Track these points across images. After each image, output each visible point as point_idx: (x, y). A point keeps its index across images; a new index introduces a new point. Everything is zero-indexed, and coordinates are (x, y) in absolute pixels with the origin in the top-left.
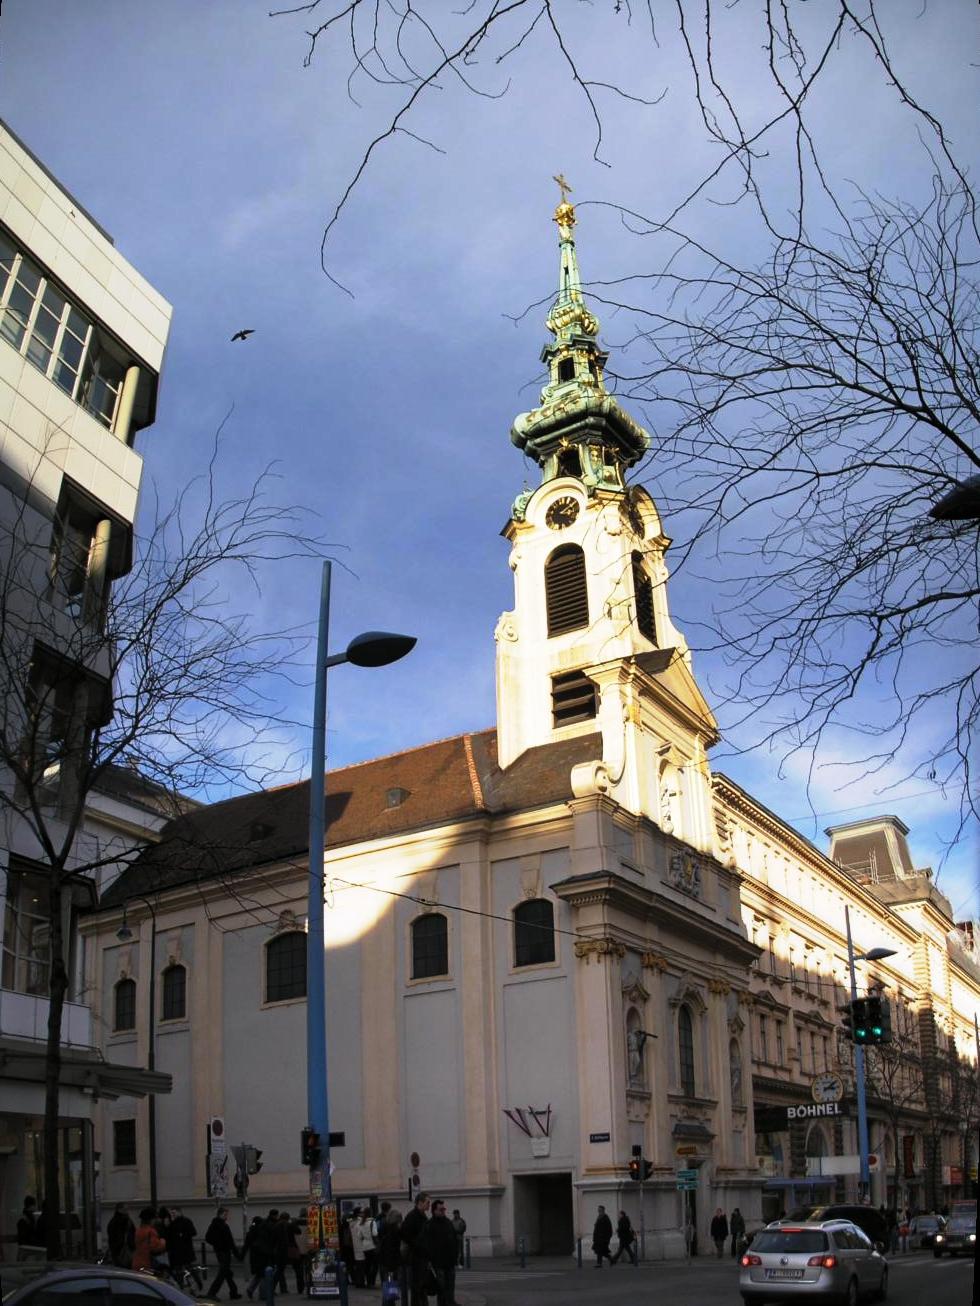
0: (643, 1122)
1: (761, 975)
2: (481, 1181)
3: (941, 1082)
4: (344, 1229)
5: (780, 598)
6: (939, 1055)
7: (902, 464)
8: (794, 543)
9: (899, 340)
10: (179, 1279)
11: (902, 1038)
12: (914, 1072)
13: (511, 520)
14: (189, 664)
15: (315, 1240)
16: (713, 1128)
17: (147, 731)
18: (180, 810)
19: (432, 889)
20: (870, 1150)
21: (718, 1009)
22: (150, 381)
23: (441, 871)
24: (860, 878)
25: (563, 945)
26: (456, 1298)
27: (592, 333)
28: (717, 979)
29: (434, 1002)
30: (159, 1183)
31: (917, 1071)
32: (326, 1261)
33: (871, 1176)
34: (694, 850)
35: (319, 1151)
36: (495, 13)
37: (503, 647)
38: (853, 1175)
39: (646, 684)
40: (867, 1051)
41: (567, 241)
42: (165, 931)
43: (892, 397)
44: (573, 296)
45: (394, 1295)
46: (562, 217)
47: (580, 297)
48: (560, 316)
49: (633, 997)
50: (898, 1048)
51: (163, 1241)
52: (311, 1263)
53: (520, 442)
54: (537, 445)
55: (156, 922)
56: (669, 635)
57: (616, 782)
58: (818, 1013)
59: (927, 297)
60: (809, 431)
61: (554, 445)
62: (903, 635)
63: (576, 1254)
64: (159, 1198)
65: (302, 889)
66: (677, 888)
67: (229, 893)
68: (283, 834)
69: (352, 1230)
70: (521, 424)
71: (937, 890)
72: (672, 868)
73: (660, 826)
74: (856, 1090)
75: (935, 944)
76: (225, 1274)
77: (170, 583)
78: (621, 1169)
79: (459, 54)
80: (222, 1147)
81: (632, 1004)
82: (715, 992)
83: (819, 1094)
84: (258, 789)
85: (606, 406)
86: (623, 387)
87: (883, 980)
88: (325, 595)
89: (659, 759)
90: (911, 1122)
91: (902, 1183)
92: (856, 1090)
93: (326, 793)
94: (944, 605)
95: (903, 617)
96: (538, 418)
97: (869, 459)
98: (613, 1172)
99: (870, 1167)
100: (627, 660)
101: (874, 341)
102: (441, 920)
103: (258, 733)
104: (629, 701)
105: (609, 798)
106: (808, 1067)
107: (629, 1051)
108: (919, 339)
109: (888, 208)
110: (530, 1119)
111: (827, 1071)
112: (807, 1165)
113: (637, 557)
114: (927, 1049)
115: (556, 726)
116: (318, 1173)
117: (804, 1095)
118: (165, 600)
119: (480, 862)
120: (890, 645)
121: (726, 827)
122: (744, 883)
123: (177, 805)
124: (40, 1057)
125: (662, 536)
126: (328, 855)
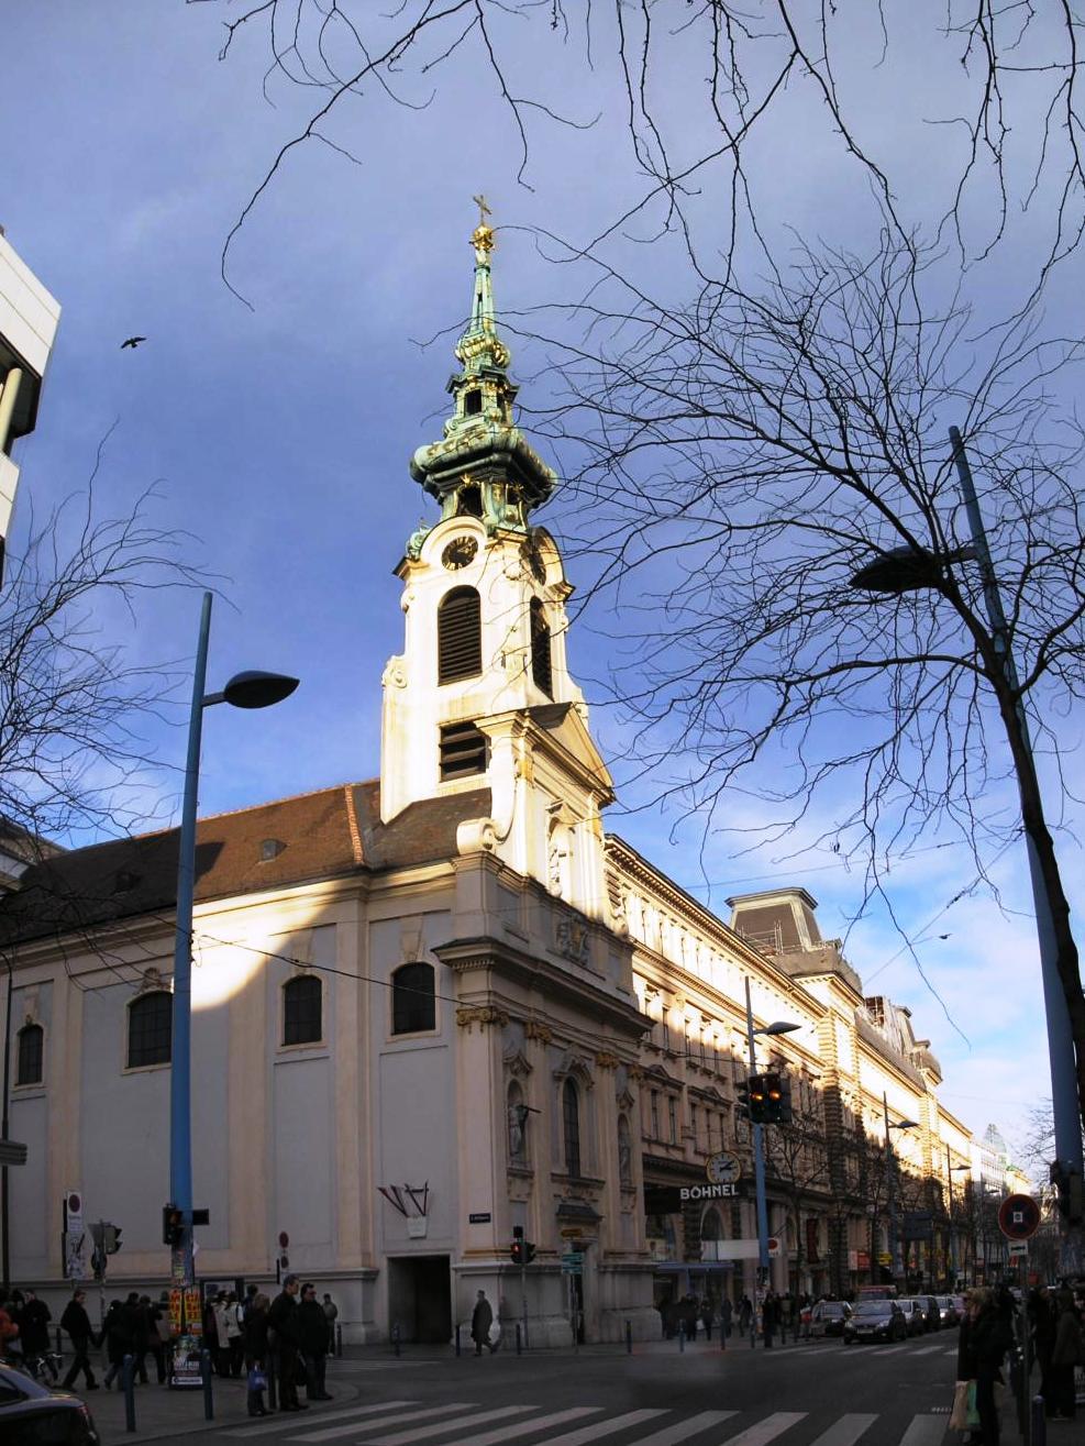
0: (524, 1202)
1: (654, 1049)
2: (354, 1263)
3: (847, 1162)
4: (208, 1314)
5: (680, 657)
6: (845, 1135)
7: (822, 525)
8: (699, 602)
9: (827, 397)
10: (33, 1367)
11: (806, 1117)
12: (818, 1152)
13: (405, 558)
14: (57, 697)
15: (177, 1325)
16: (600, 1209)
17: (10, 767)
18: (42, 855)
19: (306, 949)
20: (770, 1235)
21: (606, 1084)
22: (32, 385)
23: (319, 931)
24: (763, 949)
25: (443, 1013)
26: (327, 1389)
27: (503, 366)
28: (605, 1051)
29: (306, 1071)
30: (11, 1261)
31: (821, 1151)
32: (188, 1349)
33: (771, 1261)
34: (584, 916)
35: (182, 1230)
36: (424, 20)
37: (390, 693)
38: (752, 1260)
39: (540, 738)
40: (767, 1130)
41: (483, 266)
42: (23, 987)
43: (816, 456)
44: (486, 325)
45: (260, 1385)
46: (480, 240)
47: (493, 326)
48: (471, 345)
49: (515, 1069)
50: (801, 1128)
51: (16, 1327)
52: (173, 1350)
53: (420, 476)
54: (438, 479)
55: (13, 978)
56: (565, 688)
57: (503, 840)
58: (714, 1089)
59: (863, 355)
60: (725, 485)
61: (454, 481)
62: (811, 703)
63: (454, 1341)
64: (12, 1280)
65: (169, 945)
66: (565, 955)
67: (91, 948)
68: (150, 885)
69: (216, 1315)
70: (422, 456)
71: (845, 962)
72: (558, 935)
73: (548, 888)
74: (754, 1170)
75: (842, 1018)
76: (82, 1363)
77: (41, 608)
78: (502, 1251)
79: (383, 59)
80: (80, 1224)
81: (513, 1077)
82: (603, 1066)
83: (714, 1174)
84: (125, 835)
85: (513, 442)
86: (530, 420)
87: (786, 1056)
88: (204, 629)
89: (548, 818)
90: (814, 1204)
91: (805, 1267)
92: (754, 1170)
93: (197, 842)
94: (859, 673)
95: (812, 684)
96: (440, 452)
97: (787, 517)
98: (494, 1254)
99: (770, 1251)
100: (521, 712)
101: (801, 395)
102: (315, 982)
103: (128, 774)
104: (522, 756)
105: (494, 856)
106: (703, 1144)
107: (510, 1127)
108: (851, 398)
109: (831, 257)
110: (406, 1198)
111: (724, 1151)
112: (702, 1248)
113: (536, 604)
114: (831, 1129)
115: (443, 780)
116: (180, 1253)
117: (698, 1175)
118: (33, 627)
119: (359, 921)
120: (796, 713)
121: (619, 892)
122: (636, 952)
123: (38, 850)
125: (564, 583)
126: (197, 910)
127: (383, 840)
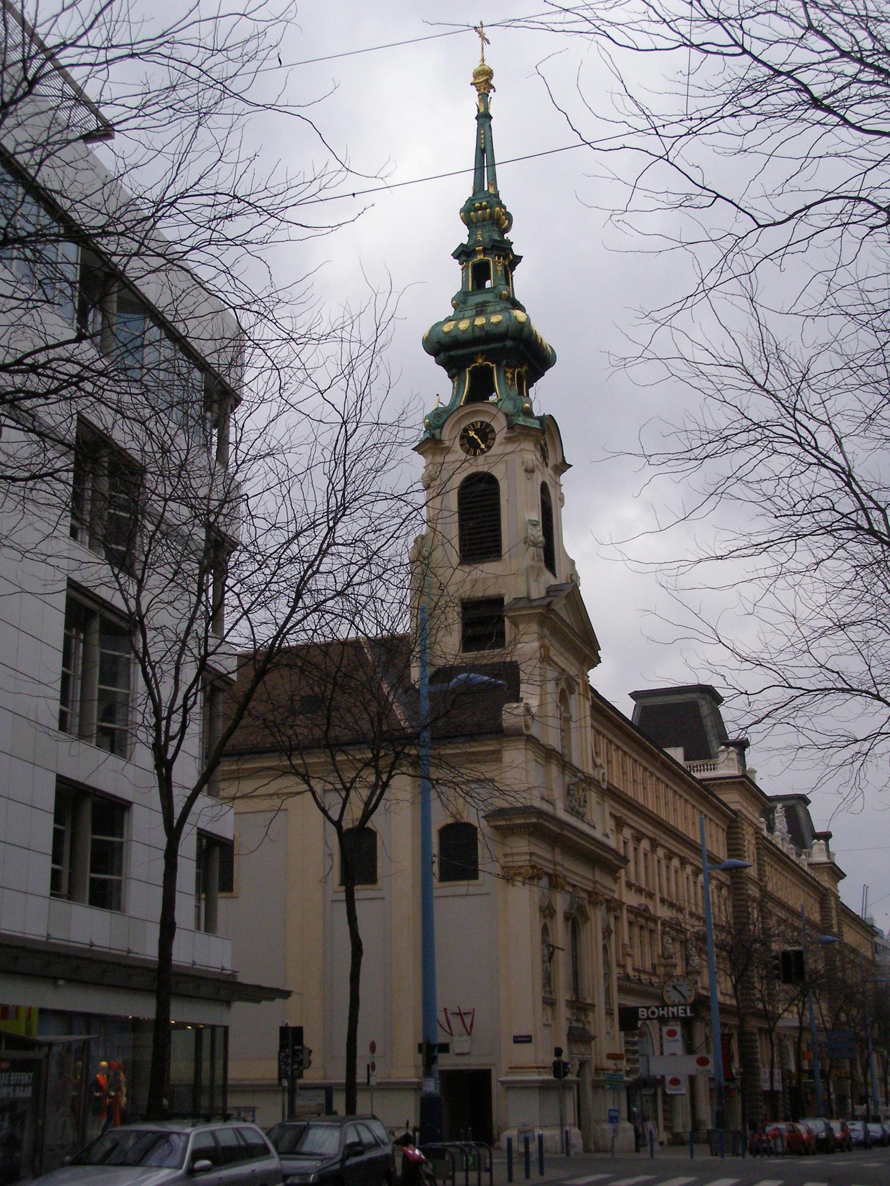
21: (597, 917)
124: (152, 970)
127: (385, 688)
